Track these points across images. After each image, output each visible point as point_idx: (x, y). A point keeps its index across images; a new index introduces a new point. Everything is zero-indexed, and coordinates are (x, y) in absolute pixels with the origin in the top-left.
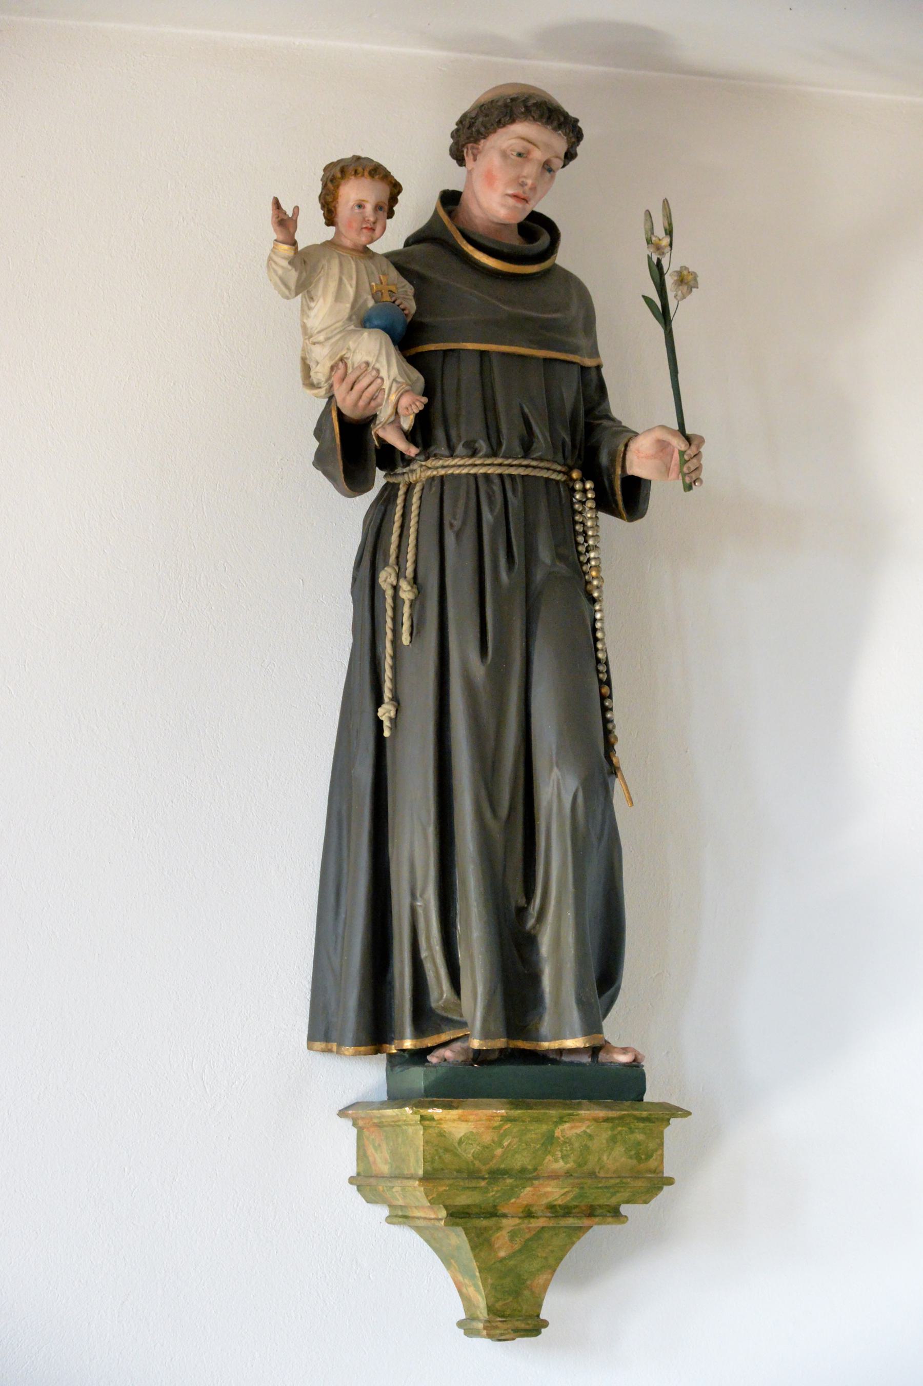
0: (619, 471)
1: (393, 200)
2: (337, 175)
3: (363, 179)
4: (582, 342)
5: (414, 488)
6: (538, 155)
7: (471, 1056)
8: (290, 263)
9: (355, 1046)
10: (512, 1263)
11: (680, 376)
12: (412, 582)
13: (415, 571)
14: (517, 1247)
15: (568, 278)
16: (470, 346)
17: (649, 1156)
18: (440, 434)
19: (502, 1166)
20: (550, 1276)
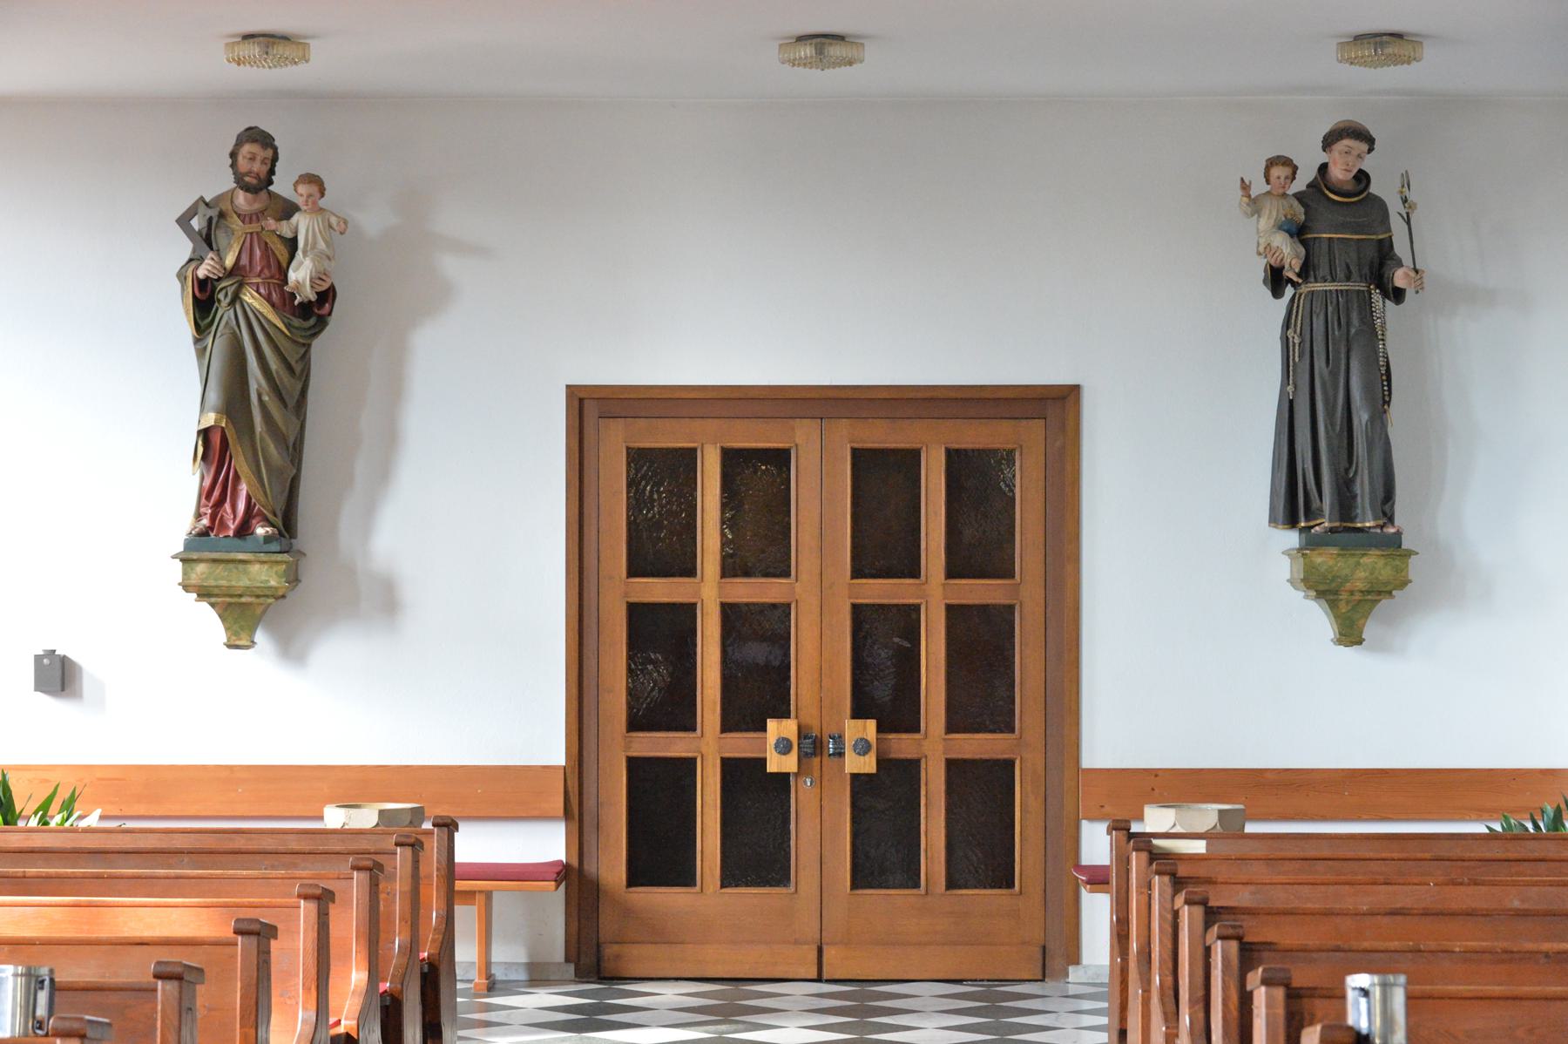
1: (1294, 173)
2: (1272, 163)
6: (1355, 153)
8: (582, 975)
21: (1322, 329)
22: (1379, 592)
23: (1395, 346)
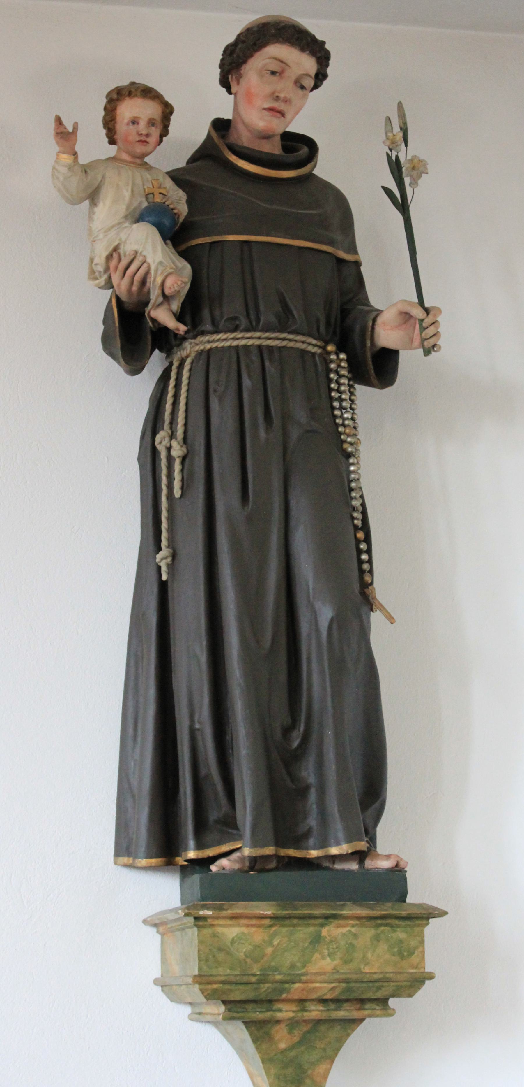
0: (369, 344)
2: (117, 96)
3: (136, 98)
4: (338, 237)
5: (185, 362)
7: (247, 864)
9: (146, 858)
10: (293, 1054)
11: (418, 257)
12: (182, 442)
13: (185, 432)
14: (296, 1039)
15: (327, 187)
16: (231, 238)
17: (411, 953)
18: (206, 313)
19: (273, 964)
20: (329, 1066)
21: (231, 425)
22: (363, 999)
23: (375, 472)
